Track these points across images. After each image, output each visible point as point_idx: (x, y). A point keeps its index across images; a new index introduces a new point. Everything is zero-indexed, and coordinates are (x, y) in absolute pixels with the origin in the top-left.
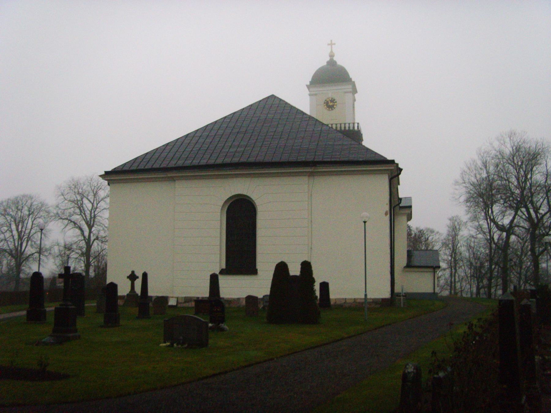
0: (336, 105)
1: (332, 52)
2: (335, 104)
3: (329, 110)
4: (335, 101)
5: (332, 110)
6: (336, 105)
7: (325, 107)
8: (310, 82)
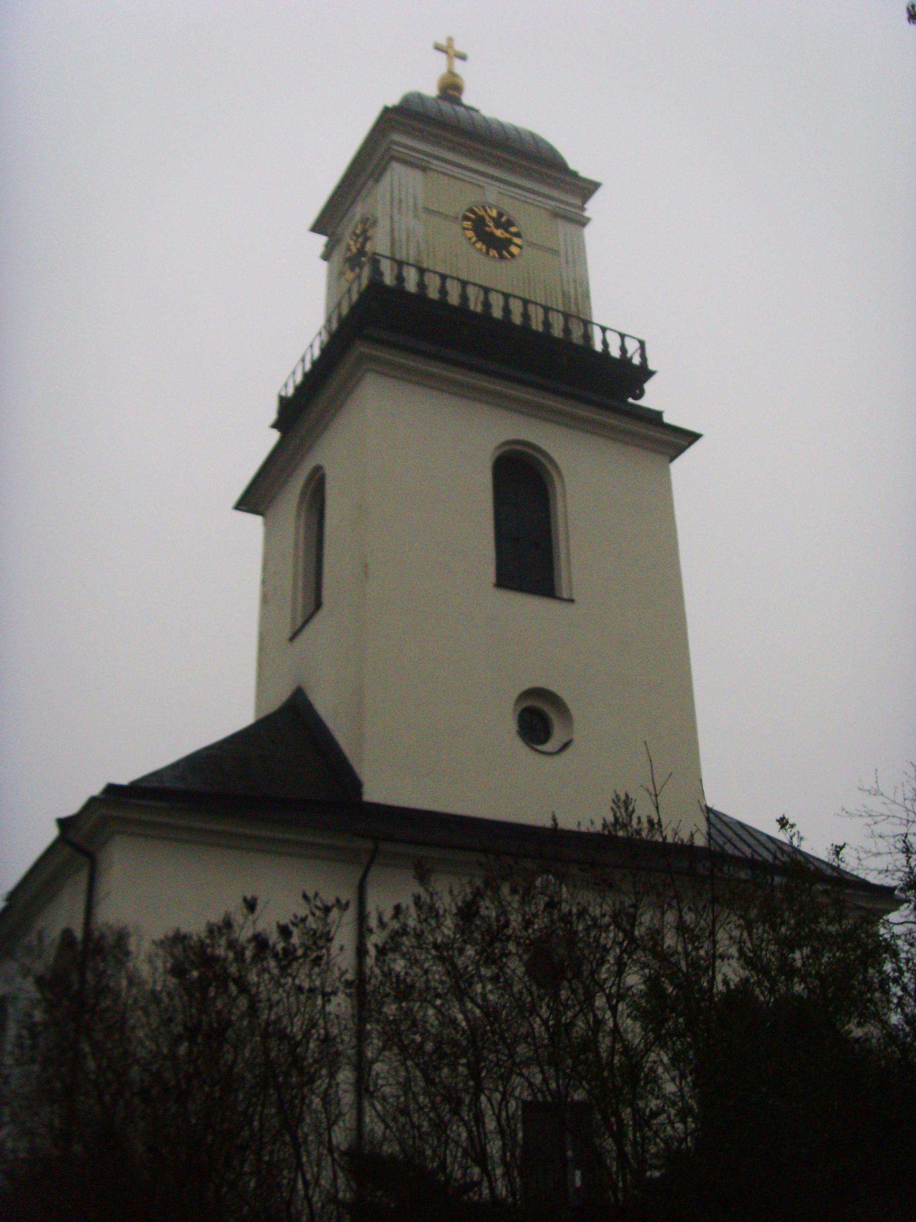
2: (517, 240)
4: (513, 229)
5: (502, 257)
6: (520, 247)
7: (470, 234)
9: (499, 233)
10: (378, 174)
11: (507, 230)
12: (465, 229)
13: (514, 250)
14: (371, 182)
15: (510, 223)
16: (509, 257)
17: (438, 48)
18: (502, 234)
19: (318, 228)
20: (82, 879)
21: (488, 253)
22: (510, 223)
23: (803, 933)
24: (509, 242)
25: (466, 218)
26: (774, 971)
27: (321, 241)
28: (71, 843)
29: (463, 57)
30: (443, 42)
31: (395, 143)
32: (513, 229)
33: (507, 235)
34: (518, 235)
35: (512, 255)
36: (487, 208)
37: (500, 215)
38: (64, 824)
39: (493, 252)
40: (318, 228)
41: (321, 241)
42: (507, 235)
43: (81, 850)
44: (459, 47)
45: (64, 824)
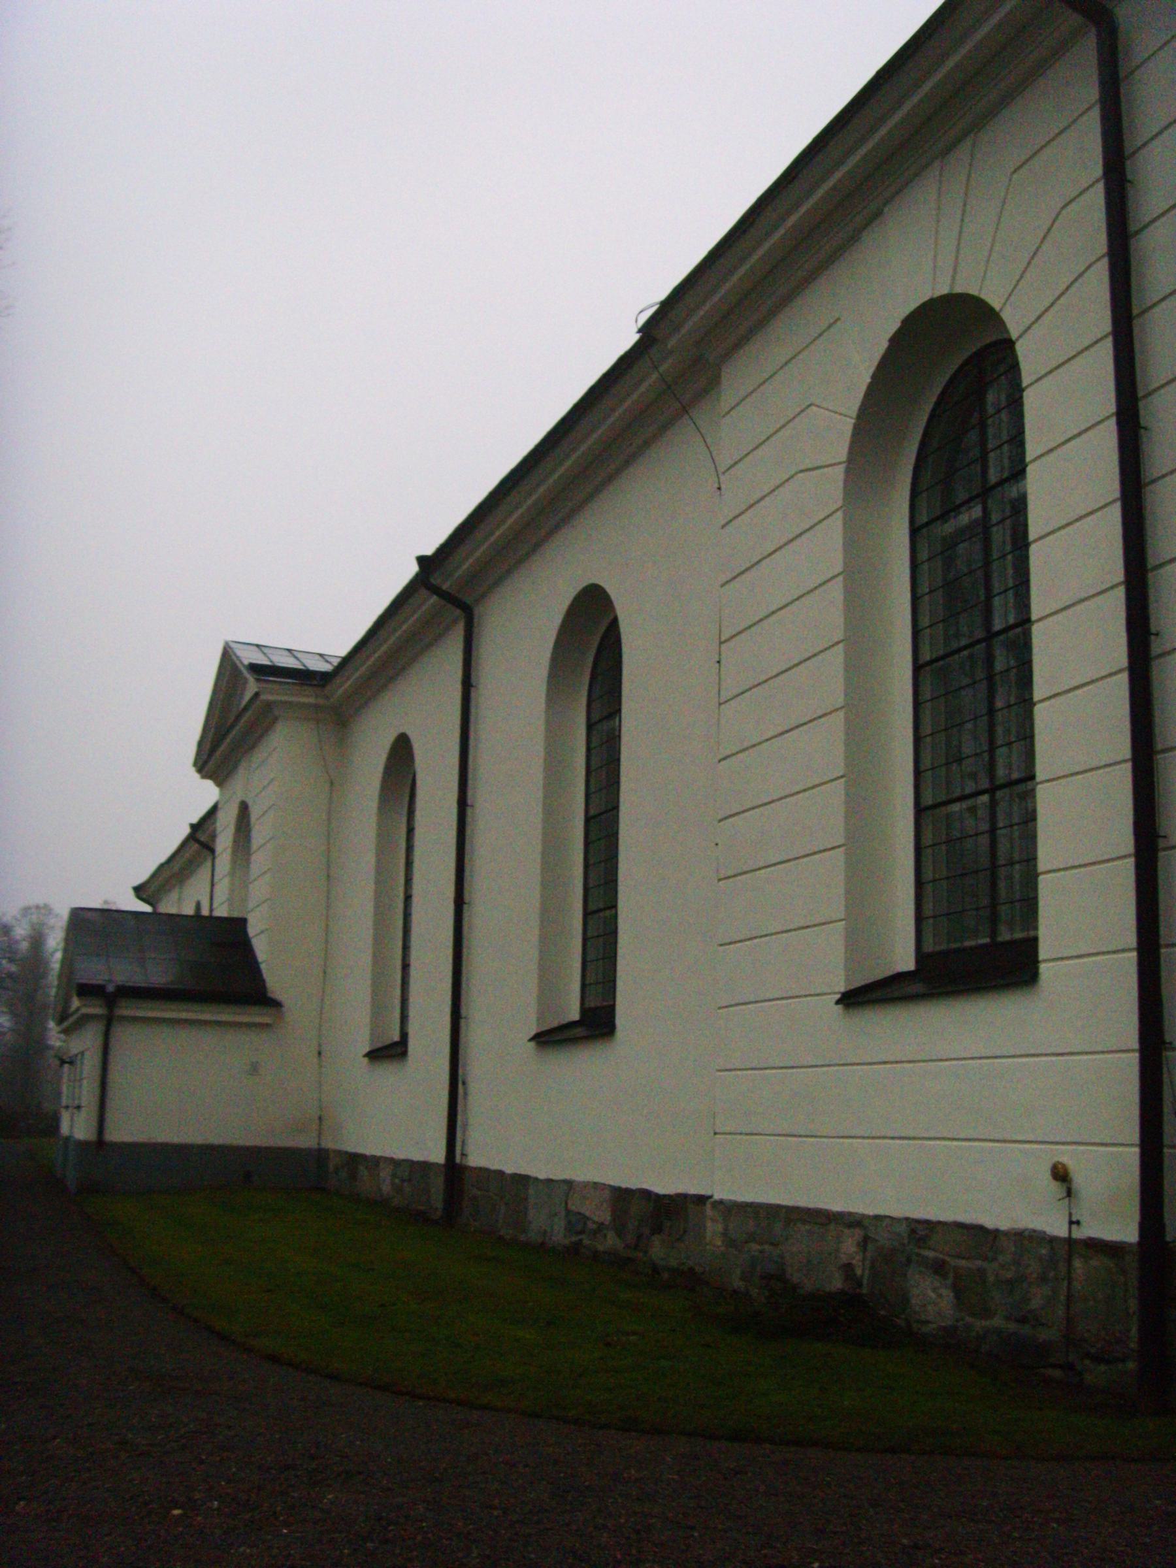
38: (421, 560)
45: (421, 560)
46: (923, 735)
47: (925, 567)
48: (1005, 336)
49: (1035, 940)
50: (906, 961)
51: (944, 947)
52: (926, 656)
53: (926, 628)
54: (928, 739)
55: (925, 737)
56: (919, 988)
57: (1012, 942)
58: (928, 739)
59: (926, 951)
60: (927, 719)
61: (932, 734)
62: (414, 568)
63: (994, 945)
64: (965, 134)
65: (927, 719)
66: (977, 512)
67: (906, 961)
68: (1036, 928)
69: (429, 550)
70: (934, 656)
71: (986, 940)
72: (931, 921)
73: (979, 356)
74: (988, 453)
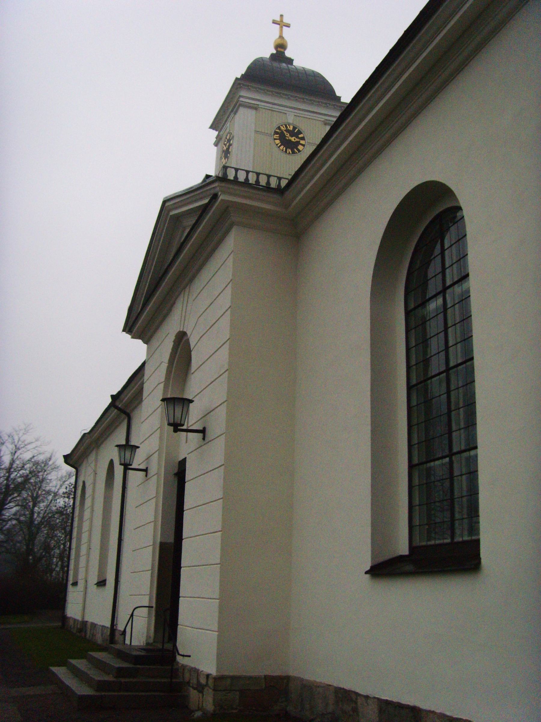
0: (304, 145)
1: (281, 37)
2: (302, 142)
3: (286, 151)
4: (300, 136)
5: (293, 152)
6: (304, 145)
7: (278, 142)
8: (132, 338)
9: (293, 139)
10: (235, 111)
11: (297, 137)
12: (275, 139)
13: (300, 147)
14: (232, 115)
15: (300, 132)
16: (297, 152)
17: (274, 22)
18: (295, 139)
19: (213, 126)
20: (126, 422)
21: (286, 151)
22: (300, 132)
23: (48, 555)
24: (298, 143)
25: (276, 133)
26: (57, 558)
27: (214, 133)
28: (117, 408)
29: (288, 26)
30: (278, 19)
31: (242, 97)
32: (300, 136)
33: (297, 140)
34: (303, 139)
35: (299, 151)
36: (288, 126)
37: (294, 128)
38: (113, 397)
39: (289, 151)
40: (213, 126)
41: (214, 133)
42: (297, 140)
43: (122, 411)
44: (285, 20)
45: (113, 397)
46: (413, 485)
47: (415, 427)
48: (456, 205)
49: (478, 542)
50: (403, 549)
51: (424, 543)
52: (416, 461)
53: (415, 406)
54: (415, 408)
55: (413, 366)
56: (409, 568)
57: (464, 542)
58: (414, 367)
59: (414, 463)
60: (415, 436)
61: (418, 443)
62: (110, 400)
63: (452, 543)
64: (187, 285)
65: (415, 436)
66: (440, 301)
67: (403, 549)
68: (478, 534)
69: (115, 393)
70: (417, 305)
71: (448, 541)
72: (414, 367)
73: (439, 217)
74: (446, 269)
